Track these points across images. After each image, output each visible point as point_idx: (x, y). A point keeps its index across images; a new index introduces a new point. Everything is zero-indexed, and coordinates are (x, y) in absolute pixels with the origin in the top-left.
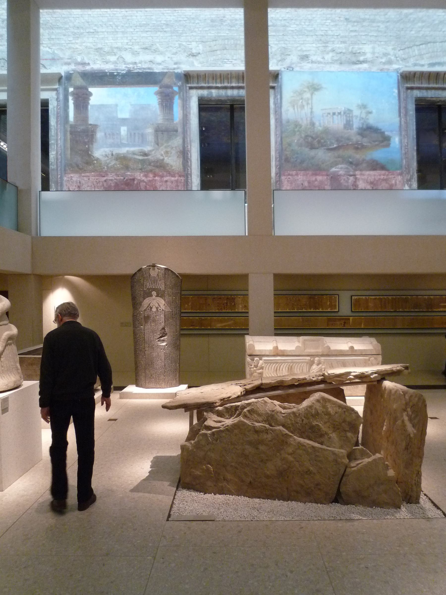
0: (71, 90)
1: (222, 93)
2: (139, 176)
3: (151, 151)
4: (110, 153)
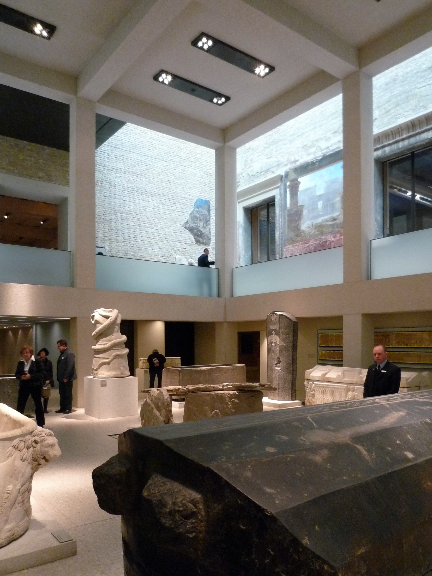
0: (288, 184)
1: (394, 147)
2: (330, 238)
3: (338, 216)
4: (311, 224)
